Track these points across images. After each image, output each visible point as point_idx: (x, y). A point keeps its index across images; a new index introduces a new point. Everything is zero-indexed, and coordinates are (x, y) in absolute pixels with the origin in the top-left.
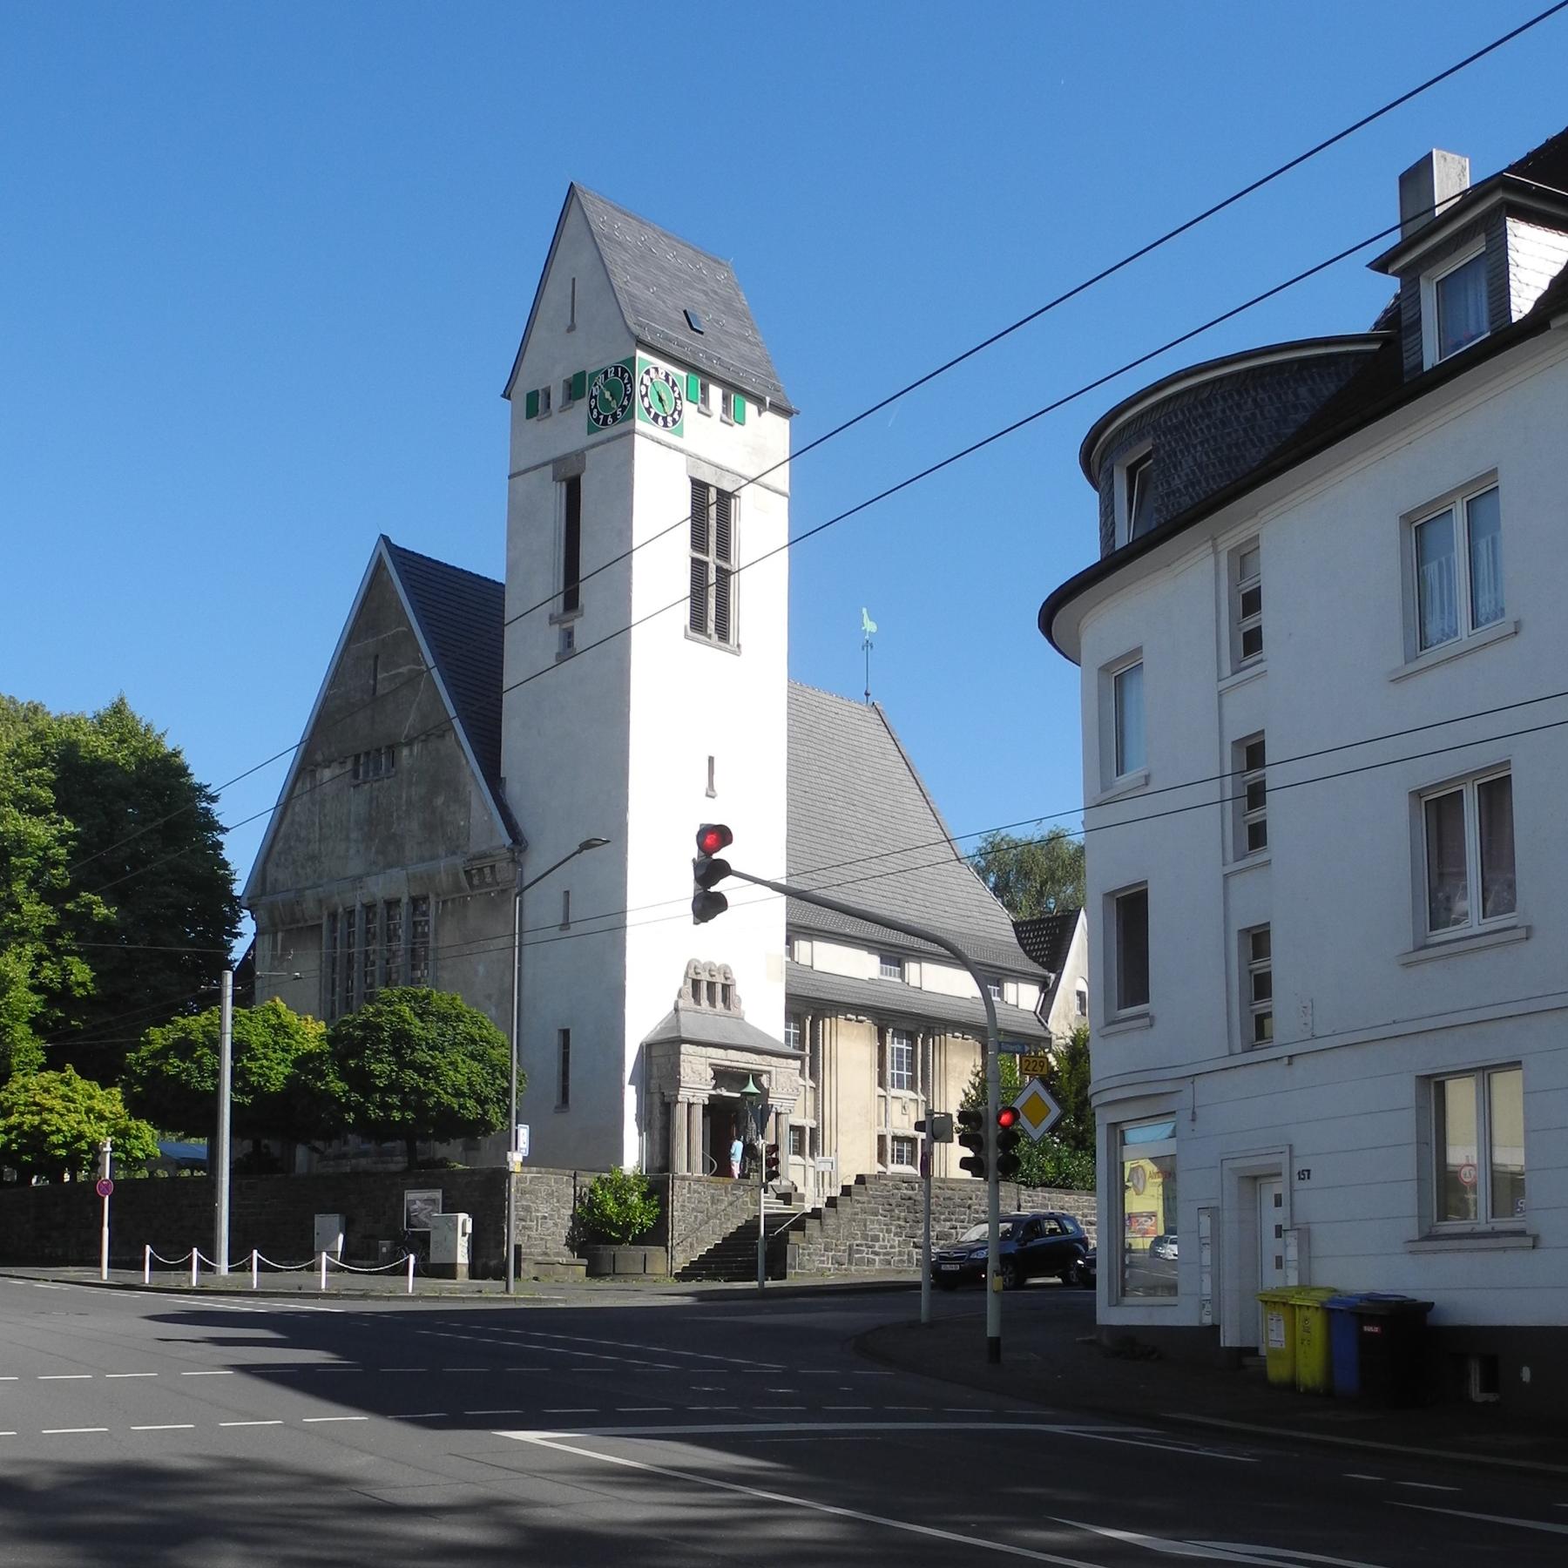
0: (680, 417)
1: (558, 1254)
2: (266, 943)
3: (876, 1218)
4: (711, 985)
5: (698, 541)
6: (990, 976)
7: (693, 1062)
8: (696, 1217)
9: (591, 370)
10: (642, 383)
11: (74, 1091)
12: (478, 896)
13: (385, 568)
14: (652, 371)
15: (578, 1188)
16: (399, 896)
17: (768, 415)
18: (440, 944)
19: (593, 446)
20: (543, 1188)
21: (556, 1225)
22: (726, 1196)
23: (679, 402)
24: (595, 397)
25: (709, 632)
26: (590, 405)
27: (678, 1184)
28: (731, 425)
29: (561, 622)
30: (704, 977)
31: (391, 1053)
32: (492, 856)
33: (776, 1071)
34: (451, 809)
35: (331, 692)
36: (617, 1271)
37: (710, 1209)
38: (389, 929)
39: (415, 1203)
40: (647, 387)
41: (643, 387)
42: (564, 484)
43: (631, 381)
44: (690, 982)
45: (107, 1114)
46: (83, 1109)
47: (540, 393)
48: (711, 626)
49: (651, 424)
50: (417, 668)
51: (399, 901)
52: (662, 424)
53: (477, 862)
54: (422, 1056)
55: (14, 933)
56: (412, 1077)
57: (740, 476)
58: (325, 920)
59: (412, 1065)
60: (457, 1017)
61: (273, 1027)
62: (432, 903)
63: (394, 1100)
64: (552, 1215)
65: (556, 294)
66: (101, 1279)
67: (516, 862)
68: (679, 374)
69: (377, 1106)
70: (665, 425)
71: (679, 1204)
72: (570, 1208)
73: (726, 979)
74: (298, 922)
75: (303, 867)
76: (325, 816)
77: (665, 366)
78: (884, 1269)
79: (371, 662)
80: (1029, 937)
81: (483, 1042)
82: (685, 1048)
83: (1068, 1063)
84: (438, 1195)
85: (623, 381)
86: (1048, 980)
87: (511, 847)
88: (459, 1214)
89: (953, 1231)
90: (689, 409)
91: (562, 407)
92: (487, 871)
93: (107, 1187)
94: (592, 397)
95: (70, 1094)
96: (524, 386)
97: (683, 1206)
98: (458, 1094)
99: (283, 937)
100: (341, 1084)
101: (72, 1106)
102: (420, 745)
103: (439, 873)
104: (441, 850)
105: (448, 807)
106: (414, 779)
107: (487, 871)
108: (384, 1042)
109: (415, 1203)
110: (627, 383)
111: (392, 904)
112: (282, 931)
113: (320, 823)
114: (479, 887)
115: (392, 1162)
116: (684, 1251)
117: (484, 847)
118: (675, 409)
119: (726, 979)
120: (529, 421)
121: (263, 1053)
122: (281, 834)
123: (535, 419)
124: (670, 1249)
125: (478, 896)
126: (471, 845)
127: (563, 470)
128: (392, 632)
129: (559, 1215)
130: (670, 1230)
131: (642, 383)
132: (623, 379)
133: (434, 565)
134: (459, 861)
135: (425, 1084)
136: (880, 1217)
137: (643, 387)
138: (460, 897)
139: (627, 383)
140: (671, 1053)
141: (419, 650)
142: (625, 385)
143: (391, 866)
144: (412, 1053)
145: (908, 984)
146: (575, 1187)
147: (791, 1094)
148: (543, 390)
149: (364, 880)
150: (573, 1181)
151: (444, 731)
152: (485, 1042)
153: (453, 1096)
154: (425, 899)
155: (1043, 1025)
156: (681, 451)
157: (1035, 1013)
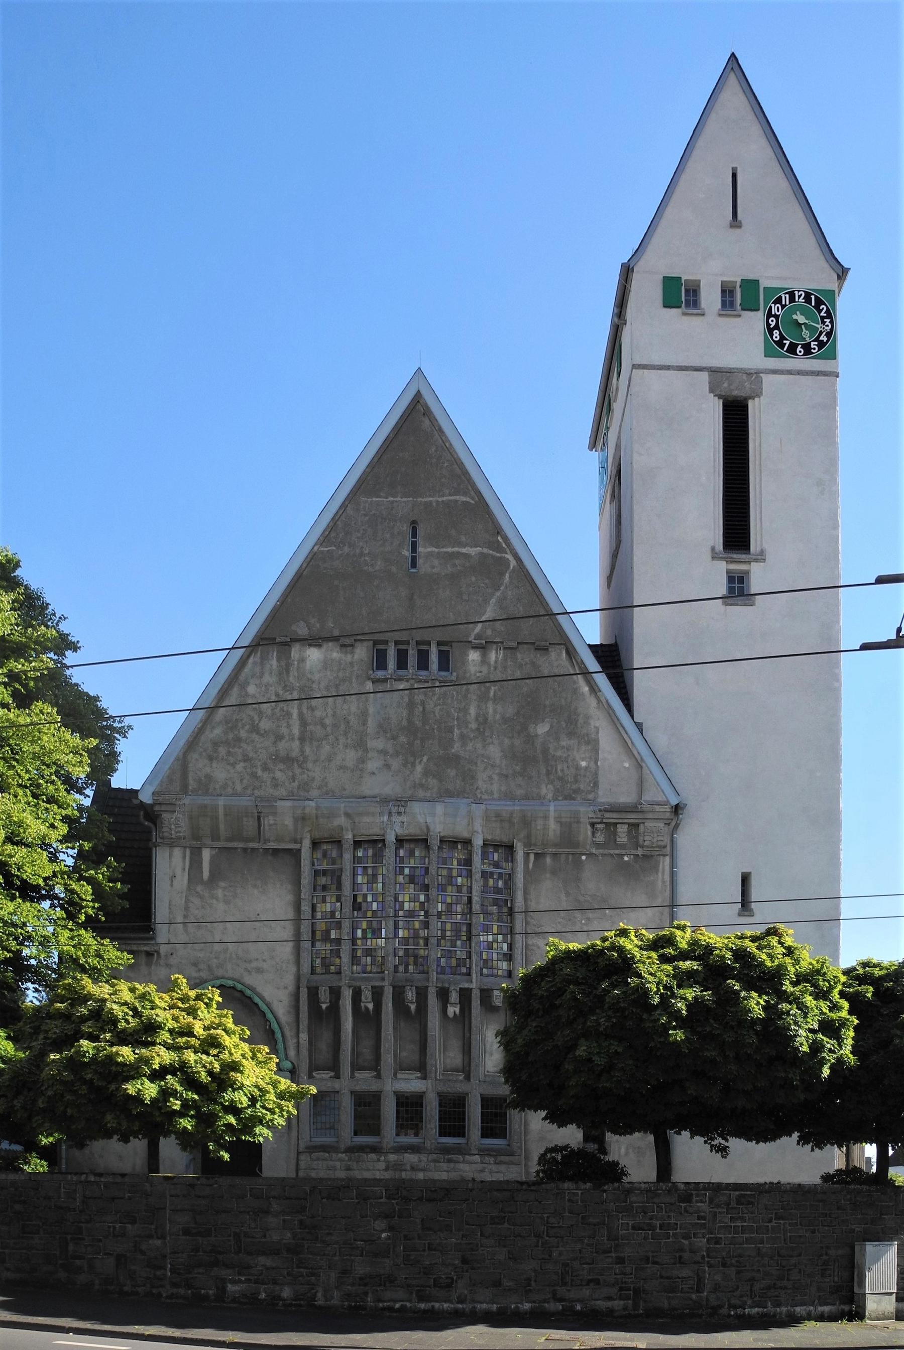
18: (533, 906)
26: (768, 325)
42: (721, 402)
53: (615, 815)
70: (792, 295)
75: (265, 768)
83: (538, 1172)
92: (622, 830)
94: (770, 315)
99: (212, 858)
103: (546, 818)
104: (546, 790)
105: (558, 739)
106: (492, 694)
107: (622, 830)
115: (464, 1162)
126: (600, 793)
127: (726, 385)
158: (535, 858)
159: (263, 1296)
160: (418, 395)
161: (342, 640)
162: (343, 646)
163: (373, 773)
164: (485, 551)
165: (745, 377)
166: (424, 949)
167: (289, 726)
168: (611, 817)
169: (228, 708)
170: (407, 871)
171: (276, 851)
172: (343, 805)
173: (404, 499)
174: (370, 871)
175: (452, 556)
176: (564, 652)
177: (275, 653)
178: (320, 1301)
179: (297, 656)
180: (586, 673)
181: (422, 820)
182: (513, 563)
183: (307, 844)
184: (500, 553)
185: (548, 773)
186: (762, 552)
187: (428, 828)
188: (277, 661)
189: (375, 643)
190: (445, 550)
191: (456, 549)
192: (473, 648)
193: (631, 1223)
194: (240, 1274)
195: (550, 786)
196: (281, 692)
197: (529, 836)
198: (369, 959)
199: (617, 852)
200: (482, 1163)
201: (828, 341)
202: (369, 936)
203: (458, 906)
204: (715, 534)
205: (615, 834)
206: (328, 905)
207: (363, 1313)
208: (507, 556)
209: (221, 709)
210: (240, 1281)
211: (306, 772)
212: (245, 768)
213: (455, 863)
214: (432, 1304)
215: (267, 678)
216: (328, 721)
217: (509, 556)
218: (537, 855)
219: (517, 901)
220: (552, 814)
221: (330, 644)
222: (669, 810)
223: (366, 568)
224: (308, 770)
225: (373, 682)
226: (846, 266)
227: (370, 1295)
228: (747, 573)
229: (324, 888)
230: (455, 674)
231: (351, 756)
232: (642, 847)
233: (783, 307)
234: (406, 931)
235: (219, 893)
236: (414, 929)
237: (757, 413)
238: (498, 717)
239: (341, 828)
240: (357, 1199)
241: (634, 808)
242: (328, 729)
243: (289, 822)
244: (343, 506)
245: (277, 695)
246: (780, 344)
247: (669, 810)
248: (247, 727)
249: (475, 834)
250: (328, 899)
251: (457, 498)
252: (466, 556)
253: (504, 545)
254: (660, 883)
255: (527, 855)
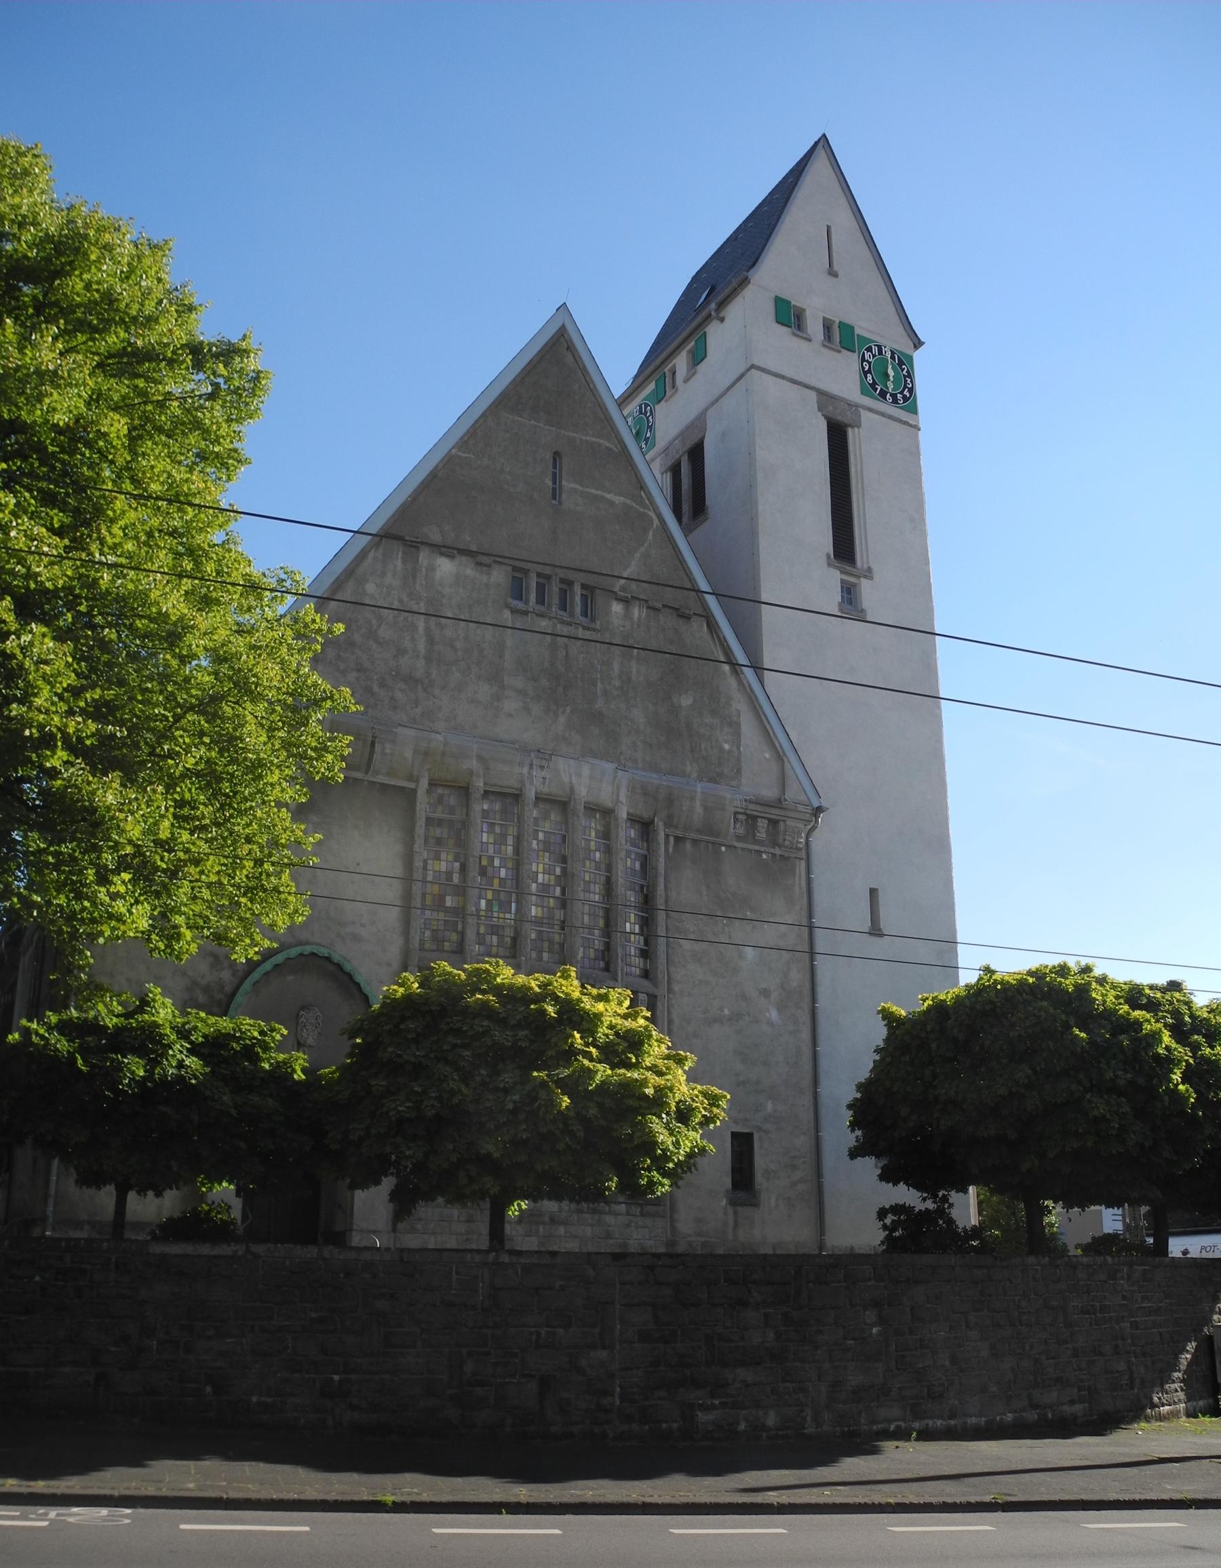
12: (739, 852)
23: (909, 380)
28: (840, 352)
40: (870, 363)
49: (879, 400)
50: (641, 510)
53: (759, 808)
55: (152, 704)
70: (895, 401)
75: (382, 685)
92: (762, 824)
94: (863, 360)
103: (692, 799)
107: (762, 824)
115: (610, 1213)
118: (905, 387)
126: (744, 781)
159: (742, 1426)
160: (563, 325)
161: (480, 558)
162: (480, 564)
163: (510, 715)
164: (629, 502)
165: (846, 406)
166: (560, 934)
167: (413, 640)
169: (341, 603)
170: (541, 836)
171: (384, 787)
172: (476, 746)
173: (547, 427)
174: (498, 830)
176: (705, 625)
177: (400, 553)
178: (810, 1429)
179: (426, 563)
181: (566, 780)
182: (656, 522)
183: (424, 783)
184: (644, 508)
185: (692, 750)
186: (869, 570)
187: (572, 789)
188: (403, 562)
189: (515, 569)
190: (589, 490)
191: (599, 493)
192: (617, 599)
193: (1080, 1305)
194: (713, 1396)
195: (695, 764)
196: (406, 599)
197: (670, 817)
198: (495, 938)
199: (757, 848)
200: (628, 1214)
201: (910, 396)
202: (496, 908)
203: (597, 885)
204: (824, 540)
206: (443, 864)
207: (858, 1440)
208: (650, 513)
209: (333, 603)
210: (714, 1407)
211: (431, 698)
212: (358, 679)
213: (593, 834)
214: (926, 1422)
215: (389, 579)
216: (459, 645)
217: (652, 514)
218: (677, 839)
219: (658, 889)
220: (699, 796)
221: (464, 558)
222: (810, 811)
223: (506, 486)
224: (434, 697)
225: (512, 612)
226: (922, 340)
227: (863, 1415)
228: (854, 585)
229: (439, 841)
230: (598, 623)
231: (485, 691)
232: (780, 846)
233: (874, 356)
234: (539, 909)
236: (549, 908)
237: (857, 442)
238: (642, 678)
239: (471, 772)
240: (845, 1282)
241: (779, 803)
242: (460, 653)
243: (408, 754)
245: (401, 601)
246: (873, 385)
247: (810, 811)
248: (363, 631)
249: (620, 804)
250: (443, 856)
251: (601, 441)
252: (611, 503)
253: (647, 502)
254: (797, 889)
255: (667, 836)
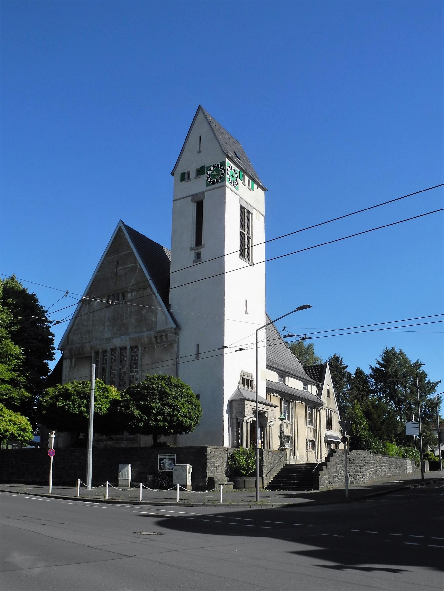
0: (237, 184)
1: (223, 480)
2: (67, 363)
3: (339, 465)
4: (248, 380)
5: (242, 226)
6: (306, 383)
7: (248, 407)
8: (270, 465)
9: (207, 165)
10: (228, 170)
11: (4, 413)
12: (159, 346)
13: (122, 231)
14: (230, 167)
15: (228, 454)
16: (126, 346)
17: (259, 189)
19: (208, 190)
20: (218, 454)
21: (222, 469)
22: (278, 457)
24: (209, 174)
25: (245, 257)
26: (207, 177)
27: (266, 453)
28: (251, 190)
29: (195, 250)
30: (246, 377)
31: (159, 399)
32: (166, 331)
33: (270, 412)
34: (149, 315)
35: (98, 274)
36: (245, 487)
37: (274, 462)
38: (121, 358)
39: (163, 460)
41: (228, 171)
42: (196, 203)
43: (224, 169)
44: (242, 378)
45: (17, 423)
46: (8, 420)
47: (186, 173)
48: (246, 255)
51: (126, 347)
52: (233, 185)
53: (161, 333)
54: (171, 401)
56: (167, 409)
57: (253, 207)
58: (93, 354)
59: (167, 404)
60: (182, 386)
61: (101, 389)
62: (140, 348)
63: (160, 418)
64: (220, 465)
65: (194, 140)
66: (49, 493)
67: (176, 334)
68: (237, 170)
69: (153, 420)
71: (266, 460)
72: (226, 462)
73: (252, 378)
74: (82, 355)
75: (85, 335)
76: (95, 317)
77: (234, 167)
78: (341, 485)
79: (115, 263)
80: (310, 371)
81: (191, 396)
82: (246, 402)
84: (175, 456)
85: (221, 169)
86: (319, 385)
87: (175, 328)
88: (188, 465)
89: (360, 470)
90: (240, 182)
91: (195, 177)
92: (164, 337)
93: (53, 453)
94: (208, 174)
95: (3, 414)
96: (180, 170)
97: (267, 461)
98: (185, 416)
100: (138, 411)
101: (4, 419)
102: (136, 292)
103: (144, 337)
104: (145, 329)
108: (156, 395)
109: (163, 460)
110: (223, 170)
111: (123, 349)
112: (74, 358)
113: (92, 319)
114: (160, 343)
116: (267, 478)
117: (163, 328)
119: (252, 378)
120: (181, 182)
121: (99, 399)
122: (76, 323)
123: (184, 182)
124: (263, 478)
125: (159, 346)
126: (158, 327)
127: (196, 198)
128: (124, 253)
129: (223, 465)
130: (263, 470)
131: (228, 170)
132: (221, 168)
133: (136, 232)
134: (152, 333)
135: (173, 412)
136: (340, 465)
137: (228, 171)
138: (151, 346)
139: (223, 170)
140: (240, 404)
141: (136, 259)
142: (222, 170)
143: (122, 335)
144: (167, 400)
145: (286, 385)
146: (227, 454)
147: (273, 420)
148: (187, 172)
149: (112, 339)
150: (226, 451)
151: (147, 287)
152: (192, 396)
153: (183, 417)
154: (137, 347)
155: (319, 400)
156: (238, 195)
157: (316, 396)
158: (144, 349)
163: (106, 332)
168: (160, 334)
175: (125, 268)
180: (154, 293)
182: (139, 266)
199: (163, 344)
205: (162, 339)
217: (138, 265)
235: (75, 370)
244: (103, 261)
252: (129, 267)
254: (174, 352)
255: (142, 348)
